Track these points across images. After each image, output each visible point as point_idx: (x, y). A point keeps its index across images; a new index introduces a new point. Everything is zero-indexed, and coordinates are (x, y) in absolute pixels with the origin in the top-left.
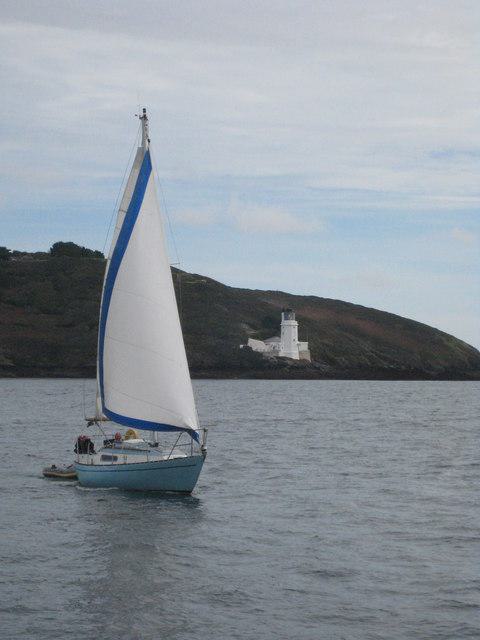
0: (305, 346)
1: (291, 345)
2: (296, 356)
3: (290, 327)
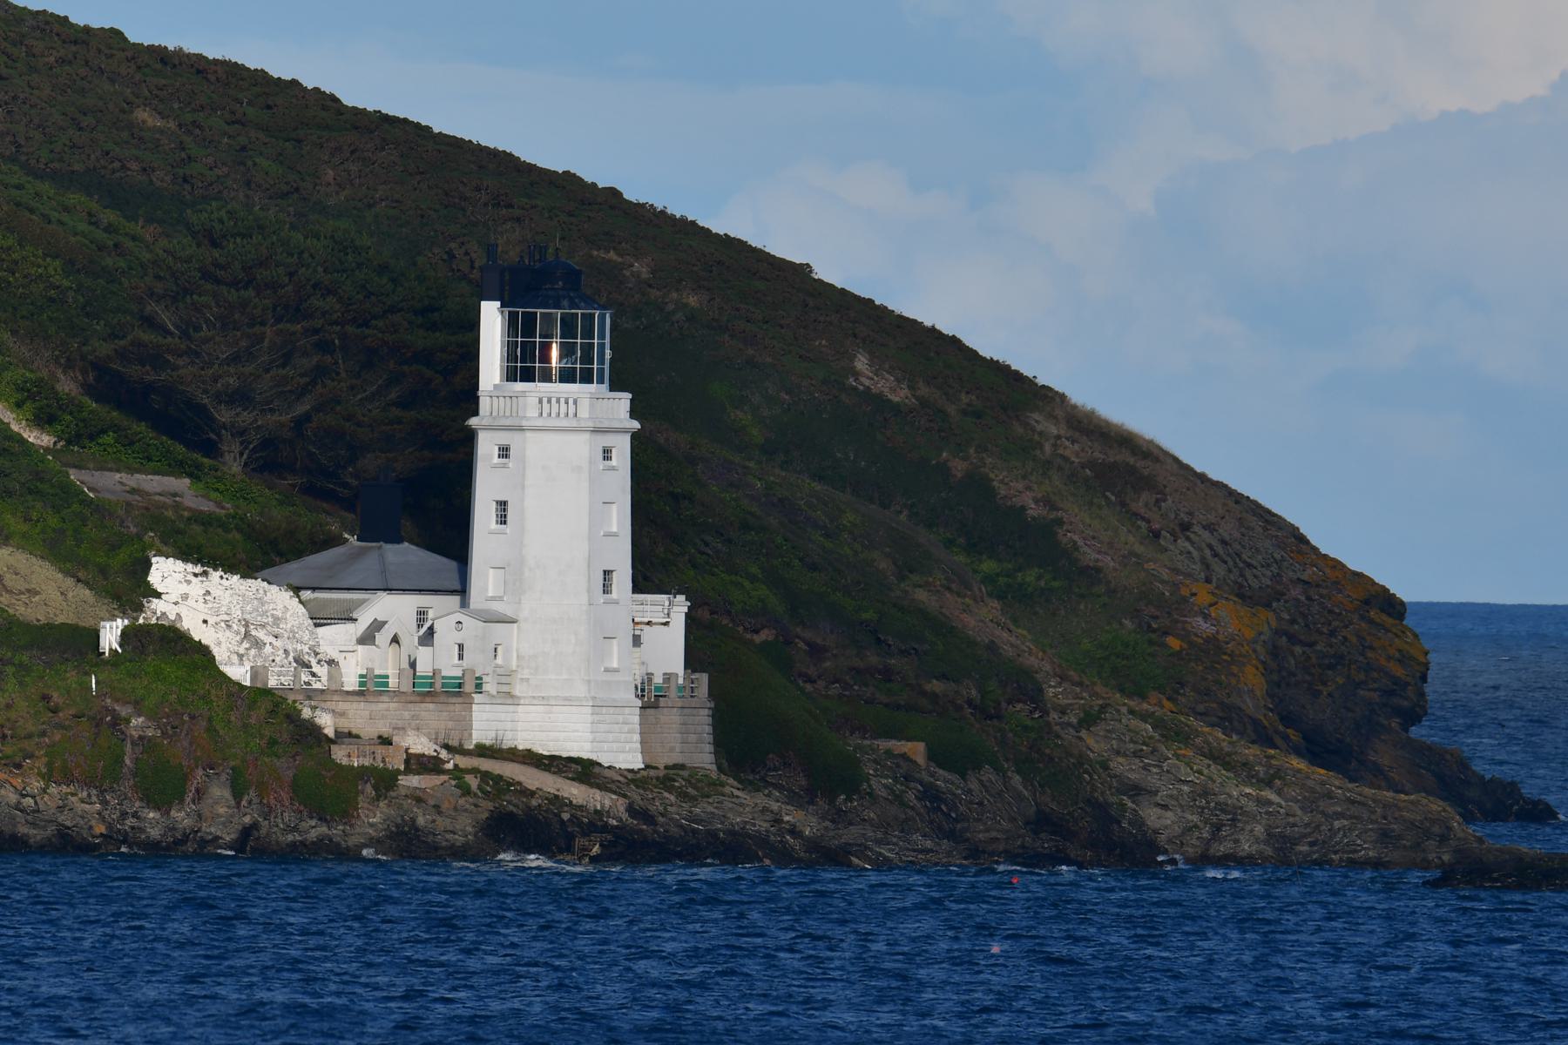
0: (668, 618)
1: (91, 466)
2: (623, 751)
3: (554, 463)
